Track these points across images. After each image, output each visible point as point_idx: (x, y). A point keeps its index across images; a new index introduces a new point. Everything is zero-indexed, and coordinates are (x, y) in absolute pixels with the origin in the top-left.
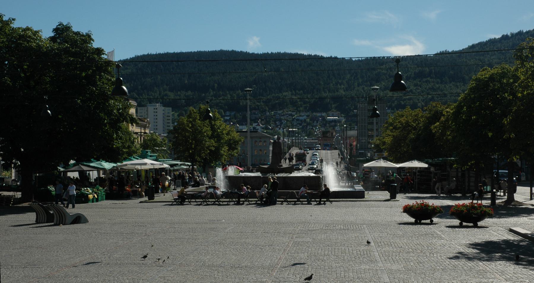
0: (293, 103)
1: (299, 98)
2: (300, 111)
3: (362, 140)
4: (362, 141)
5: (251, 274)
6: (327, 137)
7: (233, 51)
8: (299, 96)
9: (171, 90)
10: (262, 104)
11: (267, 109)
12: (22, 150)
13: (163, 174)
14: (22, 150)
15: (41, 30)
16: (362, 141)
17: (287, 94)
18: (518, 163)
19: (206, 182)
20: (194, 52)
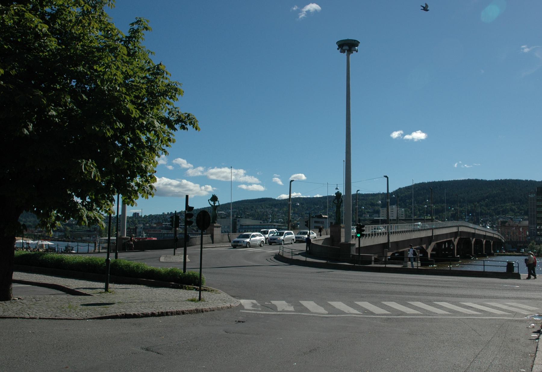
0: (512, 210)
1: (516, 207)
2: (517, 216)
3: (532, 227)
4: (531, 228)
5: (63, 306)
6: (506, 226)
7: (476, 179)
8: (517, 206)
9: (434, 204)
10: (491, 211)
11: (494, 214)
12: (99, 151)
13: (118, 161)
14: (99, 151)
15: (138, 22)
16: (531, 228)
17: (508, 205)
18: (358, 192)
19: (119, 144)
20: (530, 180)
